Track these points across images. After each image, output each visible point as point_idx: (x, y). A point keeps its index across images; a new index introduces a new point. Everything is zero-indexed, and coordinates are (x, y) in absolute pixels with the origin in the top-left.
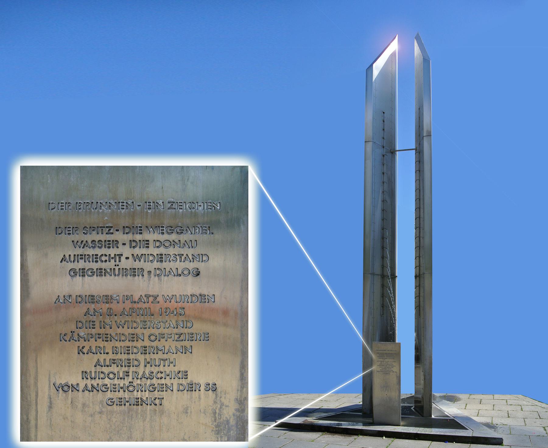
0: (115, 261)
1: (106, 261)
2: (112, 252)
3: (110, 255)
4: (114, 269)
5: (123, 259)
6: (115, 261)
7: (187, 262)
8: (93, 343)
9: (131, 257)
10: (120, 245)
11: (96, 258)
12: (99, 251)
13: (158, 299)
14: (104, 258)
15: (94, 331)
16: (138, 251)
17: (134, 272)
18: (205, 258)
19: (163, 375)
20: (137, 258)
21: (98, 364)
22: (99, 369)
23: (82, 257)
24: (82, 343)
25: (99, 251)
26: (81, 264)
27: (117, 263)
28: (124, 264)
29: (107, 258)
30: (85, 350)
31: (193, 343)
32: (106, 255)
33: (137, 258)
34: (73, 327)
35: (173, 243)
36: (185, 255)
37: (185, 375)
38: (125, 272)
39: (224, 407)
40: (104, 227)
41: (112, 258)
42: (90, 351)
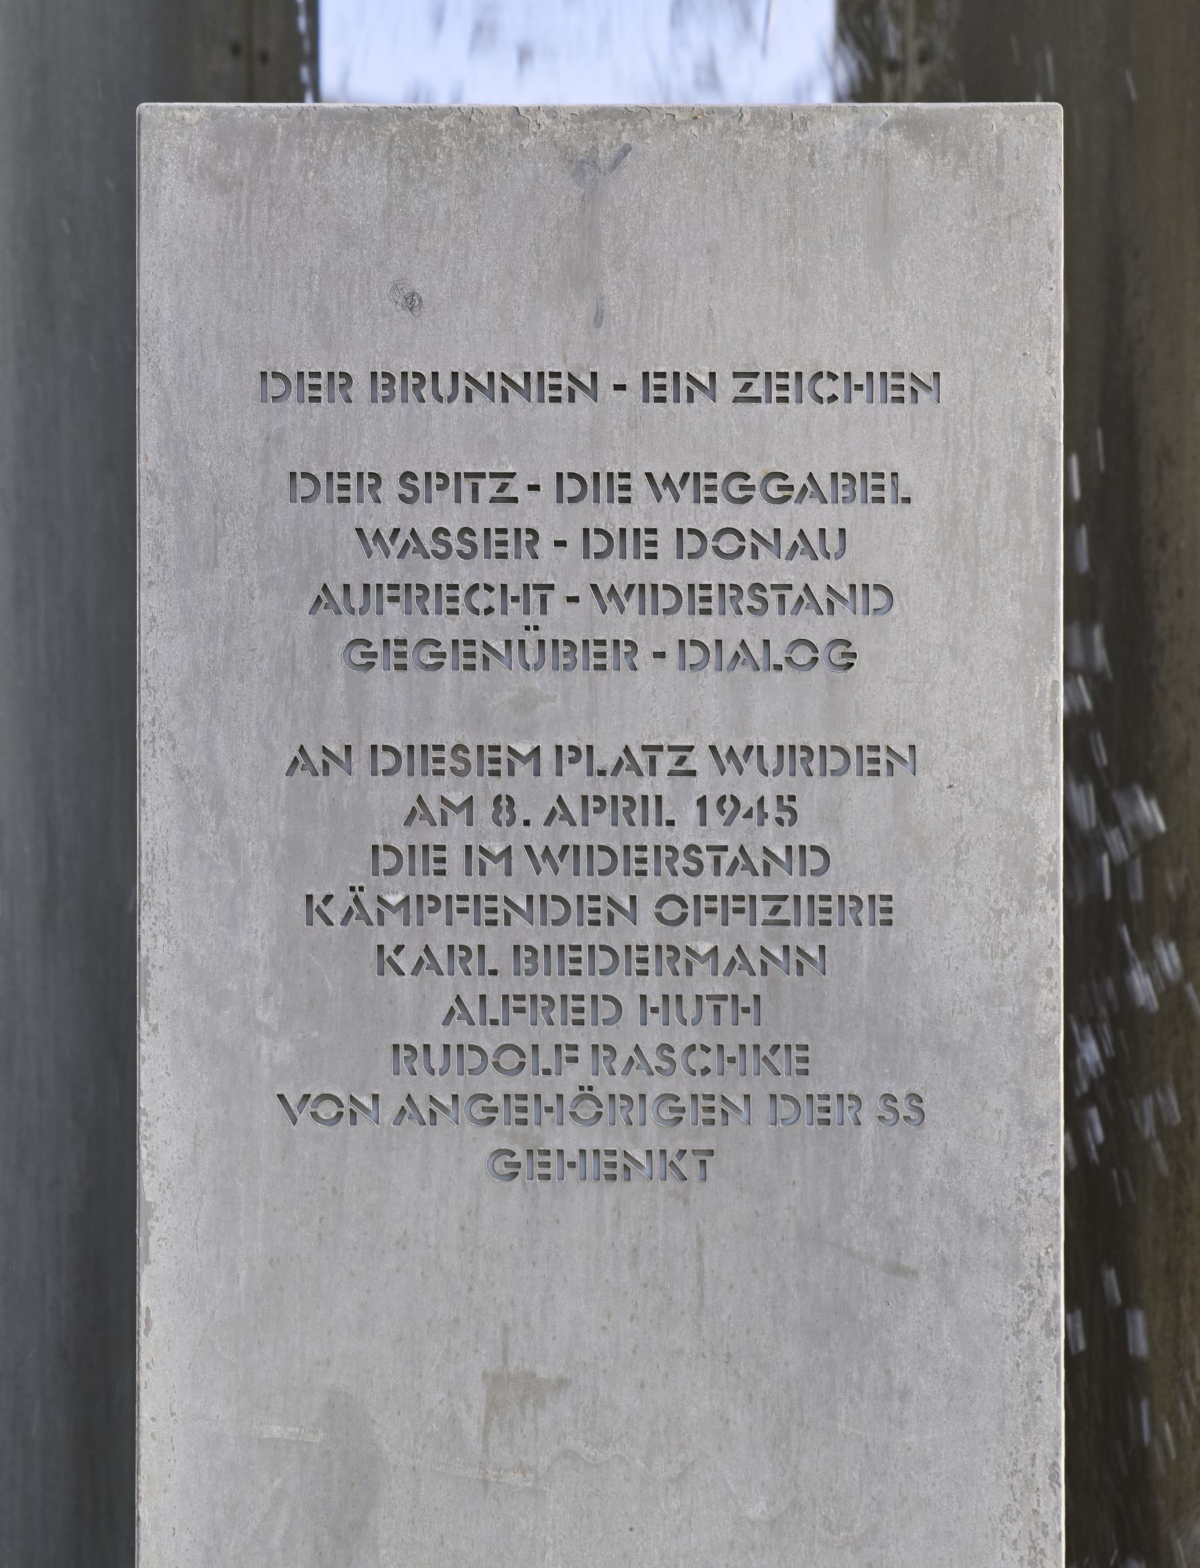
0: (527, 612)
1: (489, 610)
2: (512, 572)
3: (848, 375)
4: (522, 643)
5: (555, 600)
6: (527, 612)
7: (807, 613)
8: (440, 933)
9: (587, 596)
10: (544, 547)
11: (449, 598)
12: (465, 573)
13: (692, 763)
14: (481, 600)
15: (442, 888)
16: (621, 570)
17: (604, 655)
18: (877, 599)
19: (710, 1060)
20: (607, 597)
21: (457, 1010)
22: (461, 1033)
23: (398, 592)
24: (394, 931)
25: (465, 573)
26: (394, 621)
27: (535, 617)
28: (563, 621)
29: (838, 388)
30: (405, 962)
31: (826, 936)
32: (833, 377)
33: (607, 597)
34: (359, 871)
35: (749, 540)
36: (798, 591)
37: (801, 1058)
38: (563, 653)
39: (903, 1262)
40: (482, 475)
41: (515, 599)
42: (426, 961)
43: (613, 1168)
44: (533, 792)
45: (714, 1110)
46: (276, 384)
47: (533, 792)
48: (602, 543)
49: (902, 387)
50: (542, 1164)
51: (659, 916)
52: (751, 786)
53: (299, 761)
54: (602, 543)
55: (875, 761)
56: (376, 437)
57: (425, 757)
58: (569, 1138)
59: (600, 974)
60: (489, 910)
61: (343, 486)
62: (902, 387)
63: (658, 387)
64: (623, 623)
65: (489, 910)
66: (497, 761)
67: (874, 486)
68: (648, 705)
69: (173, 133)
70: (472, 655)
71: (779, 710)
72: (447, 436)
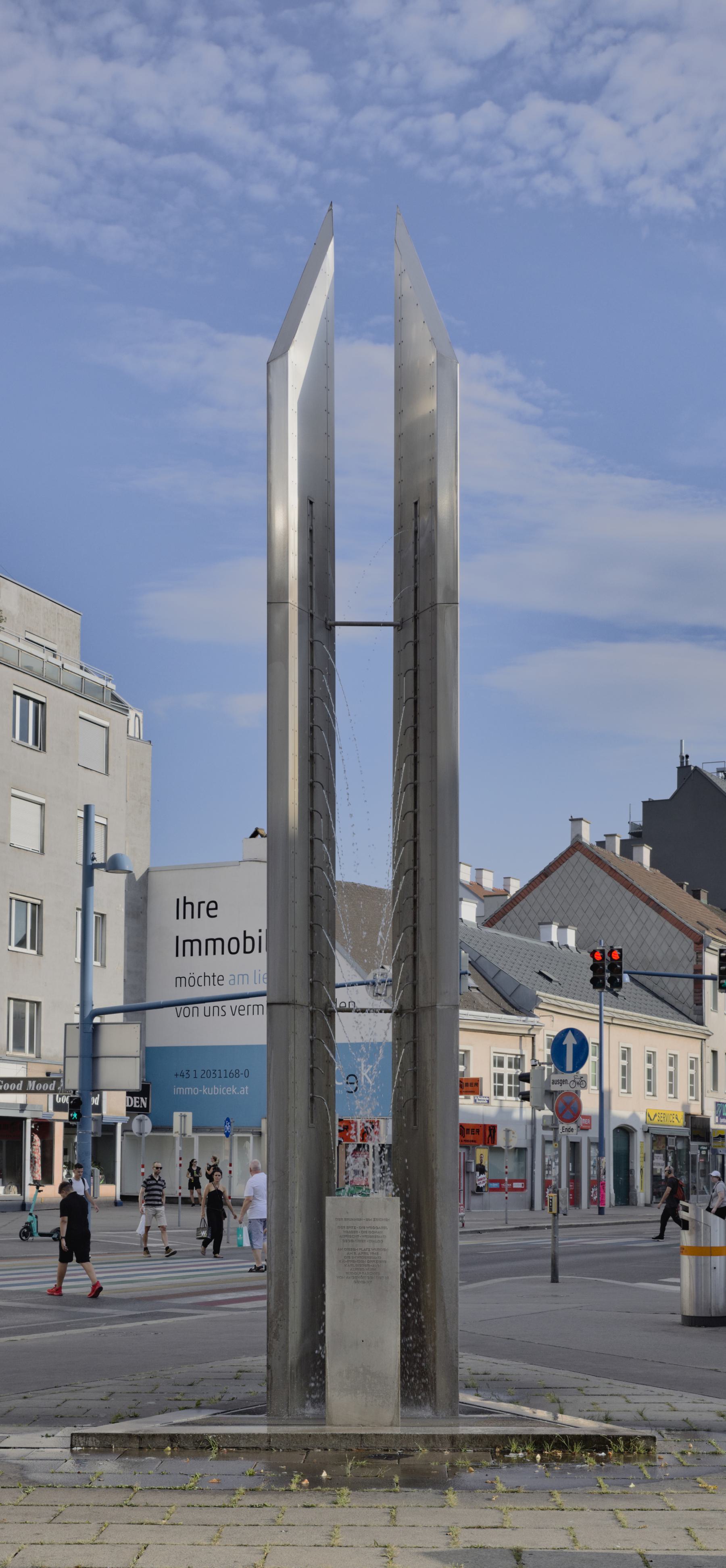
17: (363, 1241)
28: (360, 1238)
38: (359, 1241)
43: (364, 1282)
44: (357, 1252)
45: (372, 1278)
46: (337, 1219)
47: (357, 1252)
48: (363, 1232)
49: (387, 1220)
50: (358, 1282)
51: (566, 1031)
52: (375, 1252)
53: (687, 1530)
54: (363, 1232)
55: (385, 1250)
56: (345, 1224)
57: (349, 1249)
58: (360, 1280)
59: (364, 1268)
60: (354, 1261)
61: (342, 1227)
62: (387, 1220)
63: (368, 1220)
64: (364, 1238)
65: (354, 1261)
66: (354, 1249)
67: (384, 1228)
68: (366, 1245)
69: (328, 1199)
70: (352, 1241)
71: (377, 1246)
72: (350, 1223)
